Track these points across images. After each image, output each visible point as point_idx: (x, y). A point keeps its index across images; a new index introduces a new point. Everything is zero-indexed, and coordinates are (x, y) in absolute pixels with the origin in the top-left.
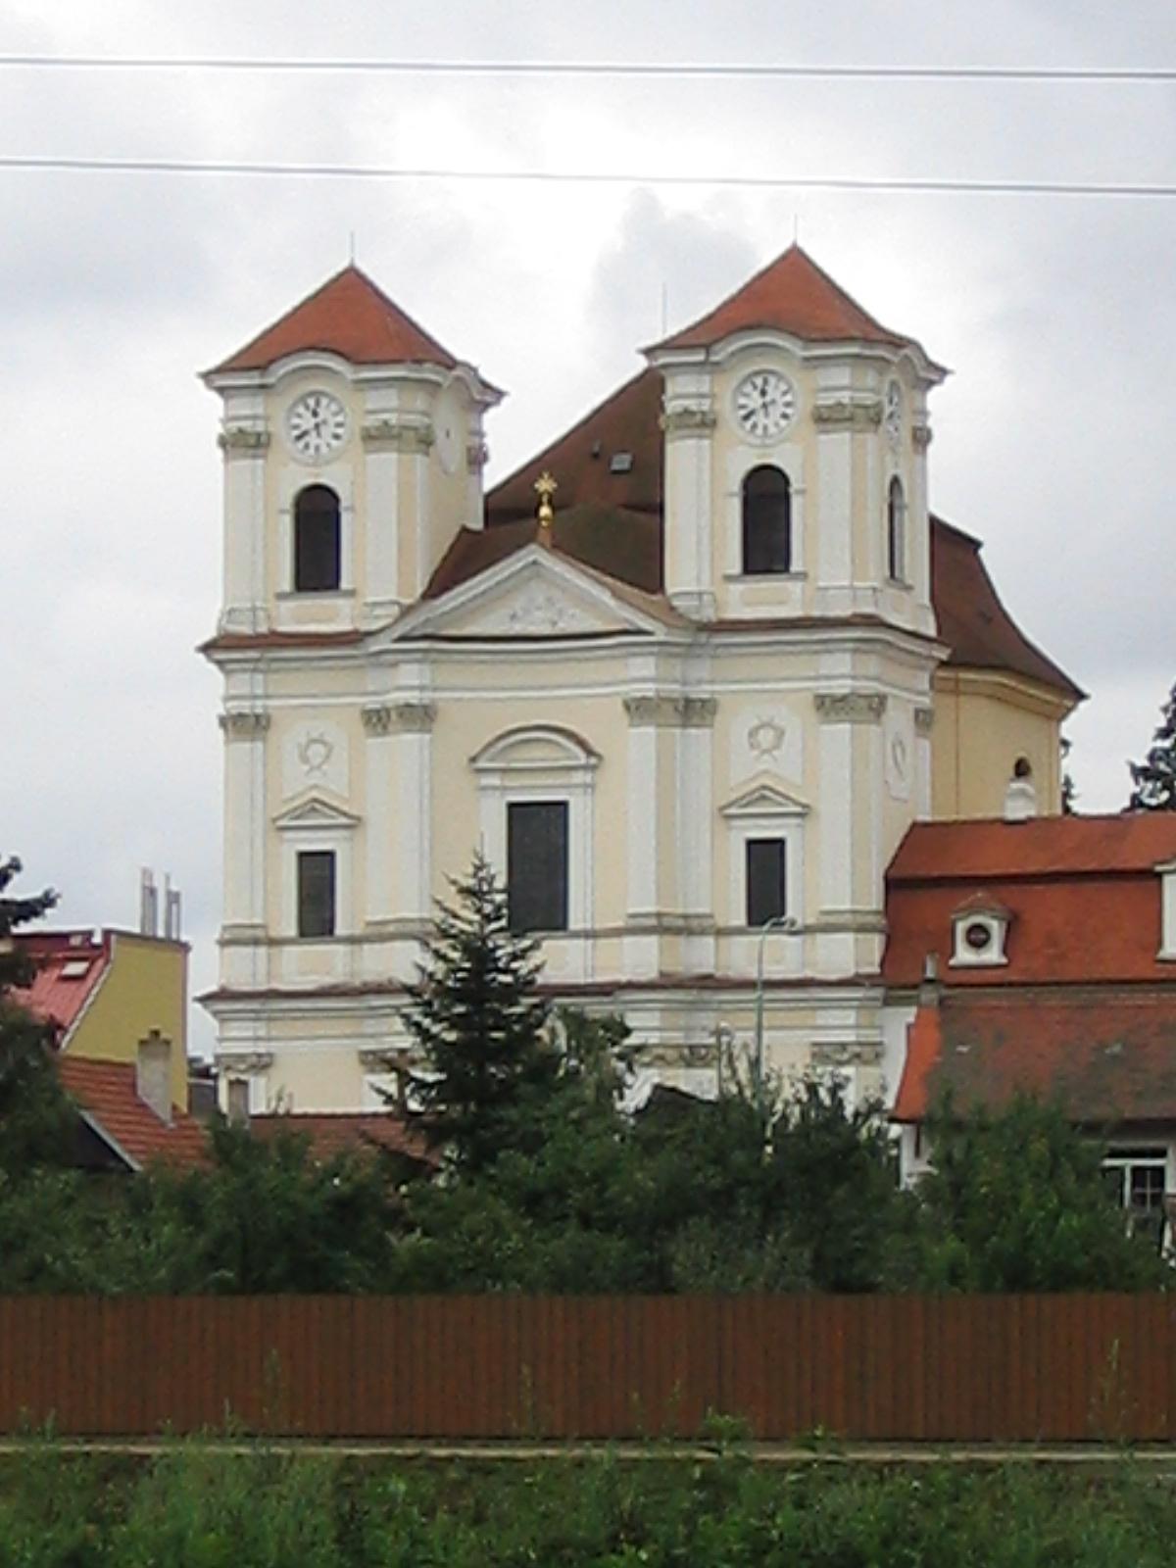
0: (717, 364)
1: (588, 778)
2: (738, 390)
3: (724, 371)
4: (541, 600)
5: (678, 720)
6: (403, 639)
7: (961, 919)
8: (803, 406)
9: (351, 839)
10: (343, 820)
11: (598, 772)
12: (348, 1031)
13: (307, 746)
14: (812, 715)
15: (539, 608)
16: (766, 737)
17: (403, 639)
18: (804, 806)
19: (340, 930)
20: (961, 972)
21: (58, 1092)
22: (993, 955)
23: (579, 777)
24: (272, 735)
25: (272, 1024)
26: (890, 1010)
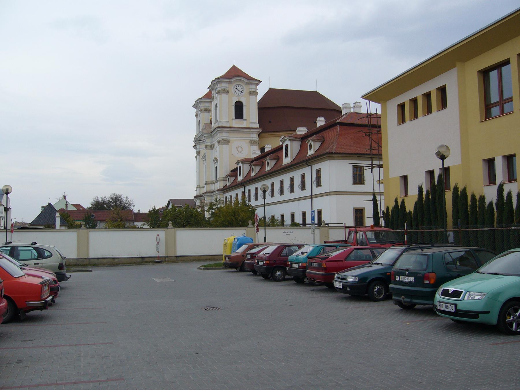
5: (210, 148)
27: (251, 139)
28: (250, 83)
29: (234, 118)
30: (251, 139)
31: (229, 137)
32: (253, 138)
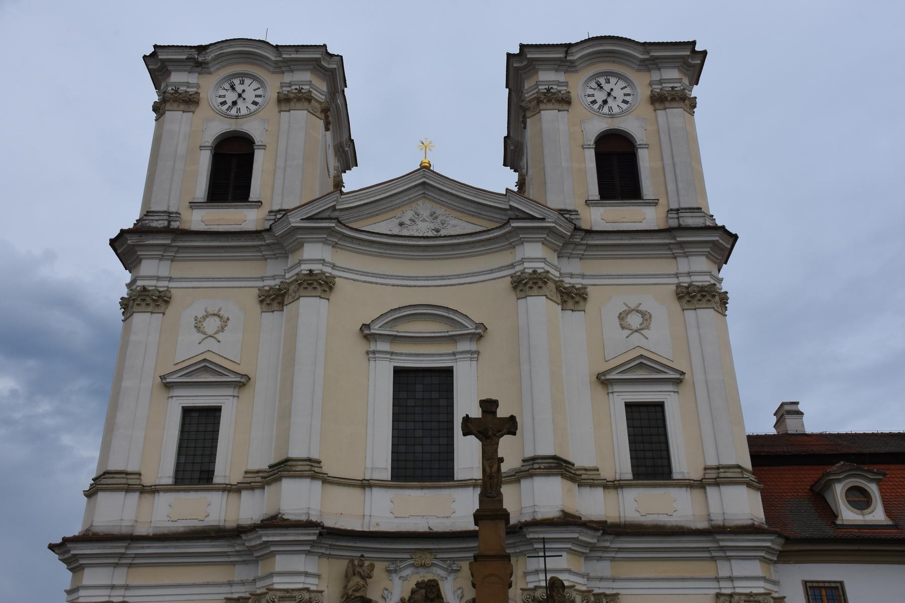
0: (572, 62)
1: (472, 346)
2: (219, 85)
3: (576, 71)
4: (425, 213)
6: (309, 219)
7: (839, 481)
8: (643, 92)
9: (194, 198)
10: (232, 378)
11: (483, 341)
12: (211, 579)
13: (205, 318)
14: (676, 306)
15: (424, 220)
16: (634, 320)
17: (309, 219)
18: (242, 376)
19: (218, 478)
20: (181, 364)
21: (520, 167)
22: (877, 515)
23: (463, 346)
24: (171, 310)
25: (132, 570)
26: (782, 567)
27: (682, 279)
28: (714, 557)
29: (598, 198)
30: (685, 280)
31: (583, 276)
32: (689, 274)
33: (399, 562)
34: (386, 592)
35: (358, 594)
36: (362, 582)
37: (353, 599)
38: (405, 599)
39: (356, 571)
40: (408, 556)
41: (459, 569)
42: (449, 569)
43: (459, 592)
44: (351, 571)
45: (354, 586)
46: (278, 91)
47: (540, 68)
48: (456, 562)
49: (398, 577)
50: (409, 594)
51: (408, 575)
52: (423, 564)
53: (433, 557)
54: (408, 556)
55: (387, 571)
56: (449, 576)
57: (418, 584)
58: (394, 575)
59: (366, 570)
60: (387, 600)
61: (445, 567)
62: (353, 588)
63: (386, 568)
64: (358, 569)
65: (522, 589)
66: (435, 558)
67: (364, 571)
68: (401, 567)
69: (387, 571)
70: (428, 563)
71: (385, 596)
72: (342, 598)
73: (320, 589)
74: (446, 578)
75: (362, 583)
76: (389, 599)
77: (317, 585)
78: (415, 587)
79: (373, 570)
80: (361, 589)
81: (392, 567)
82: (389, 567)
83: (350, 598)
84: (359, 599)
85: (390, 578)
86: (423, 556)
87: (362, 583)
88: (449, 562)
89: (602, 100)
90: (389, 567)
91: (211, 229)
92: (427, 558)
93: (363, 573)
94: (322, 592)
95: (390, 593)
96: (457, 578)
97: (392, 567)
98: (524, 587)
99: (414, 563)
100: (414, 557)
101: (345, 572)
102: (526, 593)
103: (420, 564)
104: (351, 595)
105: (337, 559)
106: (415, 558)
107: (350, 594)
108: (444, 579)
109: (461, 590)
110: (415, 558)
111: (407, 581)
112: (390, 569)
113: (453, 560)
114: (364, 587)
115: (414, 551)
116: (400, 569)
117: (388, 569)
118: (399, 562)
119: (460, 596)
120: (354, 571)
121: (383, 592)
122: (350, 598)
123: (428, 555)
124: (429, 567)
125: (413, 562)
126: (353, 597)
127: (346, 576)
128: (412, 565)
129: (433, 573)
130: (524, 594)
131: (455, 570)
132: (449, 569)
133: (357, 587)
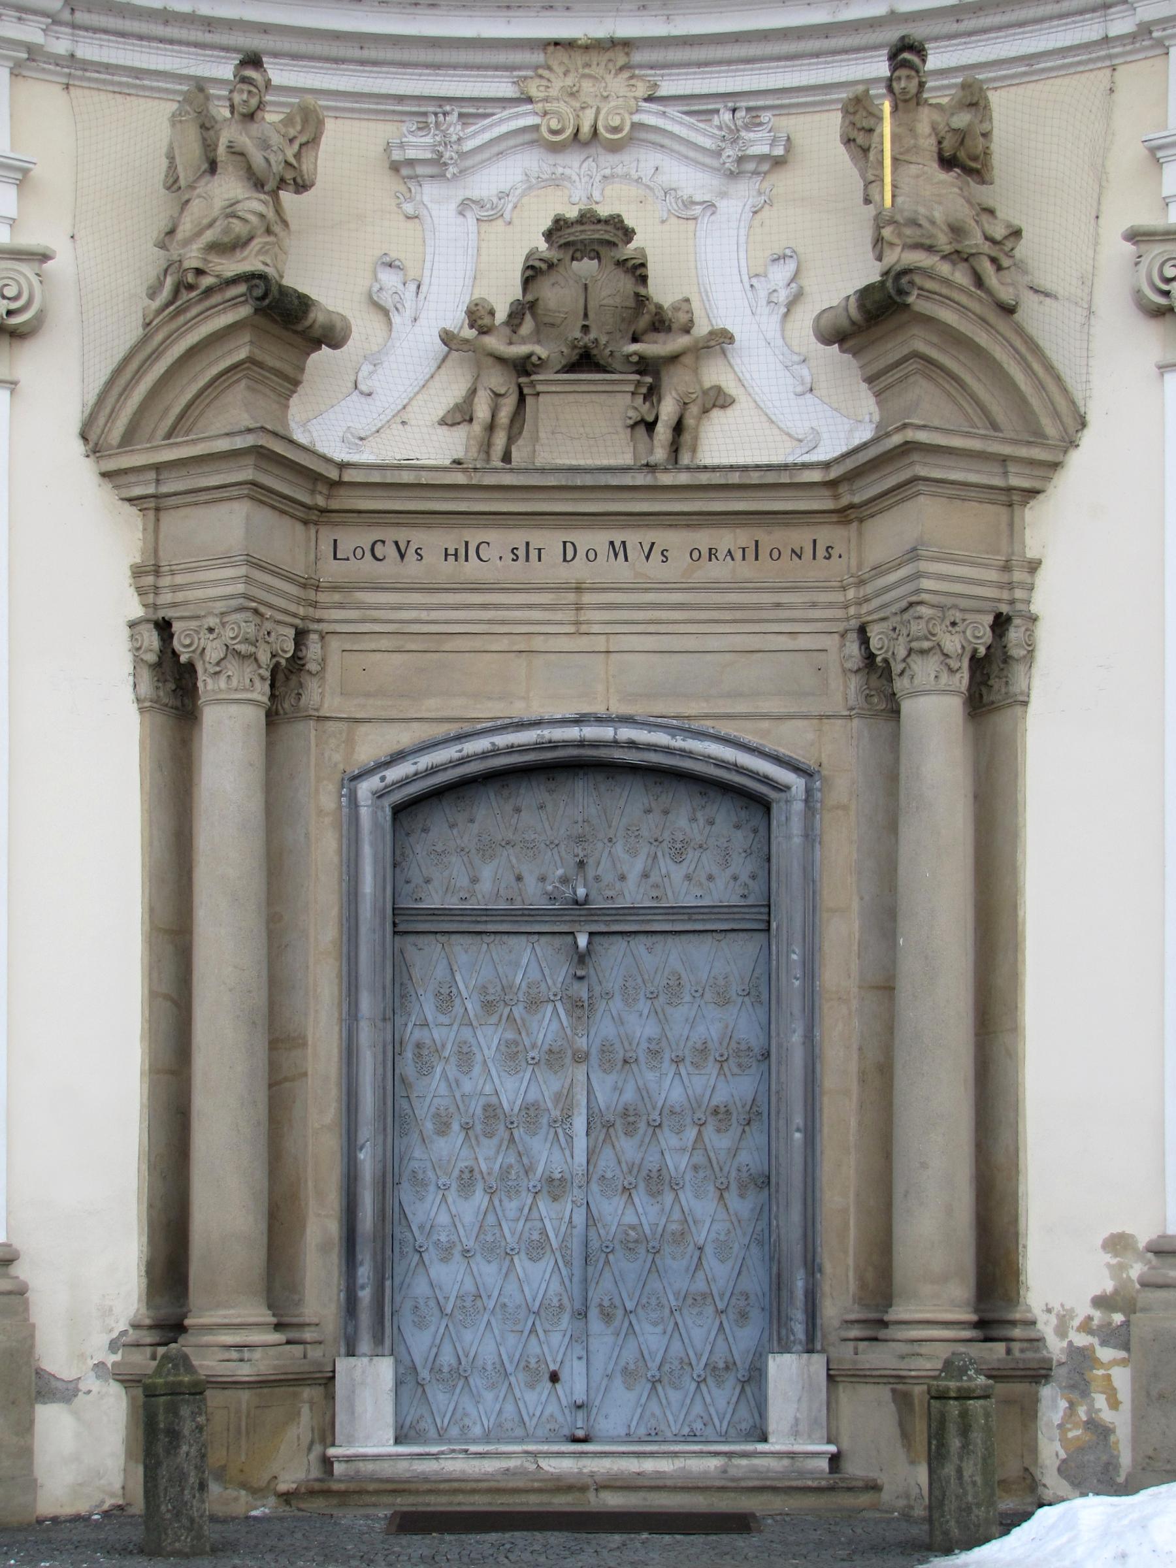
33: (453, 118)
34: (389, 279)
35: (231, 267)
36: (254, 204)
37: (209, 291)
38: (492, 313)
39: (221, 150)
40: (502, 87)
41: (779, 151)
42: (729, 152)
43: (780, 275)
44: (191, 152)
45: (210, 225)
46: (306, 196)
47: (941, 381)
48: (765, 117)
49: (453, 206)
50: (515, 291)
51: (503, 195)
52: (586, 129)
53: (641, 90)
54: (502, 87)
55: (395, 167)
56: (723, 195)
57: (557, 230)
58: (429, 192)
59: (275, 139)
60: (396, 319)
61: (708, 143)
62: (209, 236)
63: (388, 148)
64: (229, 134)
65: (1135, 236)
66: (650, 99)
67: (265, 145)
68: (469, 145)
69: (395, 167)
70: (616, 121)
71: (387, 300)
72: (152, 295)
73: (29, 240)
74: (710, 206)
75: (260, 208)
76: (408, 313)
77: (12, 223)
78: (543, 245)
79: (313, 141)
80: (251, 238)
81: (419, 146)
82: (402, 146)
83: (191, 287)
84: (242, 288)
85: (409, 208)
86: (587, 86)
87: (260, 208)
88: (727, 116)
89: (1120, 233)
90: (402, 146)
91: (428, 1505)
92: (606, 98)
93: (257, 158)
94: (44, 257)
95: (412, 287)
96: (769, 203)
97: (419, 146)
98: (1148, 219)
99: (536, 128)
100: (533, 92)
101: (165, 163)
102: (1156, 251)
103: (569, 132)
104: (199, 272)
105: (121, 91)
106: (546, 100)
107: (187, 264)
108: (698, 210)
109: (791, 266)
110: (546, 100)
111: (500, 222)
112: (411, 154)
113: (749, 109)
114: (269, 231)
115: (538, 57)
116: (462, 155)
117: (397, 155)
118: (453, 118)
119: (783, 296)
120: (209, 147)
121: (376, 279)
122: (191, 287)
123: (617, 85)
124: (615, 147)
125: (535, 120)
126: (207, 281)
127: (172, 184)
128: (531, 137)
129: (639, 180)
130: (1145, 262)
131: (762, 158)
132: (729, 152)
133: (227, 230)
